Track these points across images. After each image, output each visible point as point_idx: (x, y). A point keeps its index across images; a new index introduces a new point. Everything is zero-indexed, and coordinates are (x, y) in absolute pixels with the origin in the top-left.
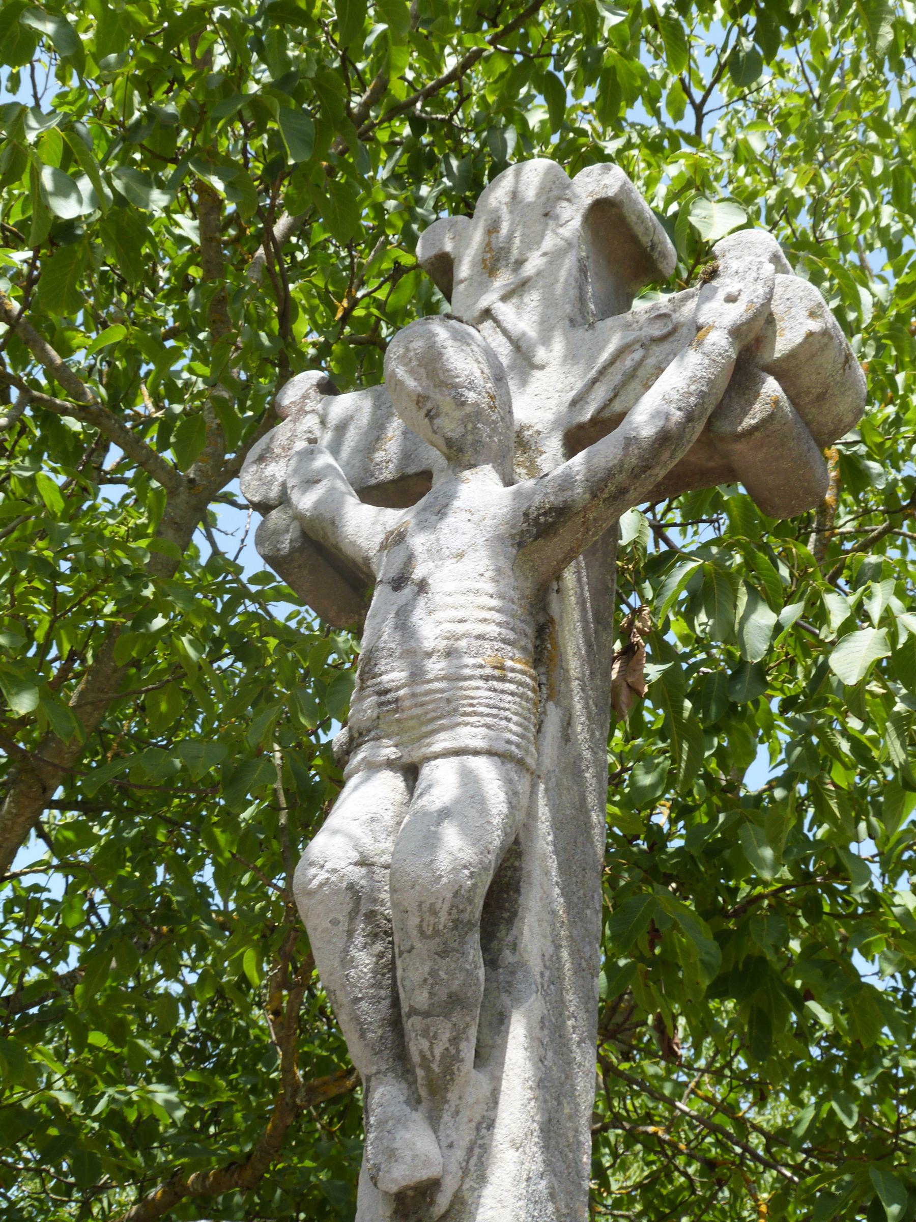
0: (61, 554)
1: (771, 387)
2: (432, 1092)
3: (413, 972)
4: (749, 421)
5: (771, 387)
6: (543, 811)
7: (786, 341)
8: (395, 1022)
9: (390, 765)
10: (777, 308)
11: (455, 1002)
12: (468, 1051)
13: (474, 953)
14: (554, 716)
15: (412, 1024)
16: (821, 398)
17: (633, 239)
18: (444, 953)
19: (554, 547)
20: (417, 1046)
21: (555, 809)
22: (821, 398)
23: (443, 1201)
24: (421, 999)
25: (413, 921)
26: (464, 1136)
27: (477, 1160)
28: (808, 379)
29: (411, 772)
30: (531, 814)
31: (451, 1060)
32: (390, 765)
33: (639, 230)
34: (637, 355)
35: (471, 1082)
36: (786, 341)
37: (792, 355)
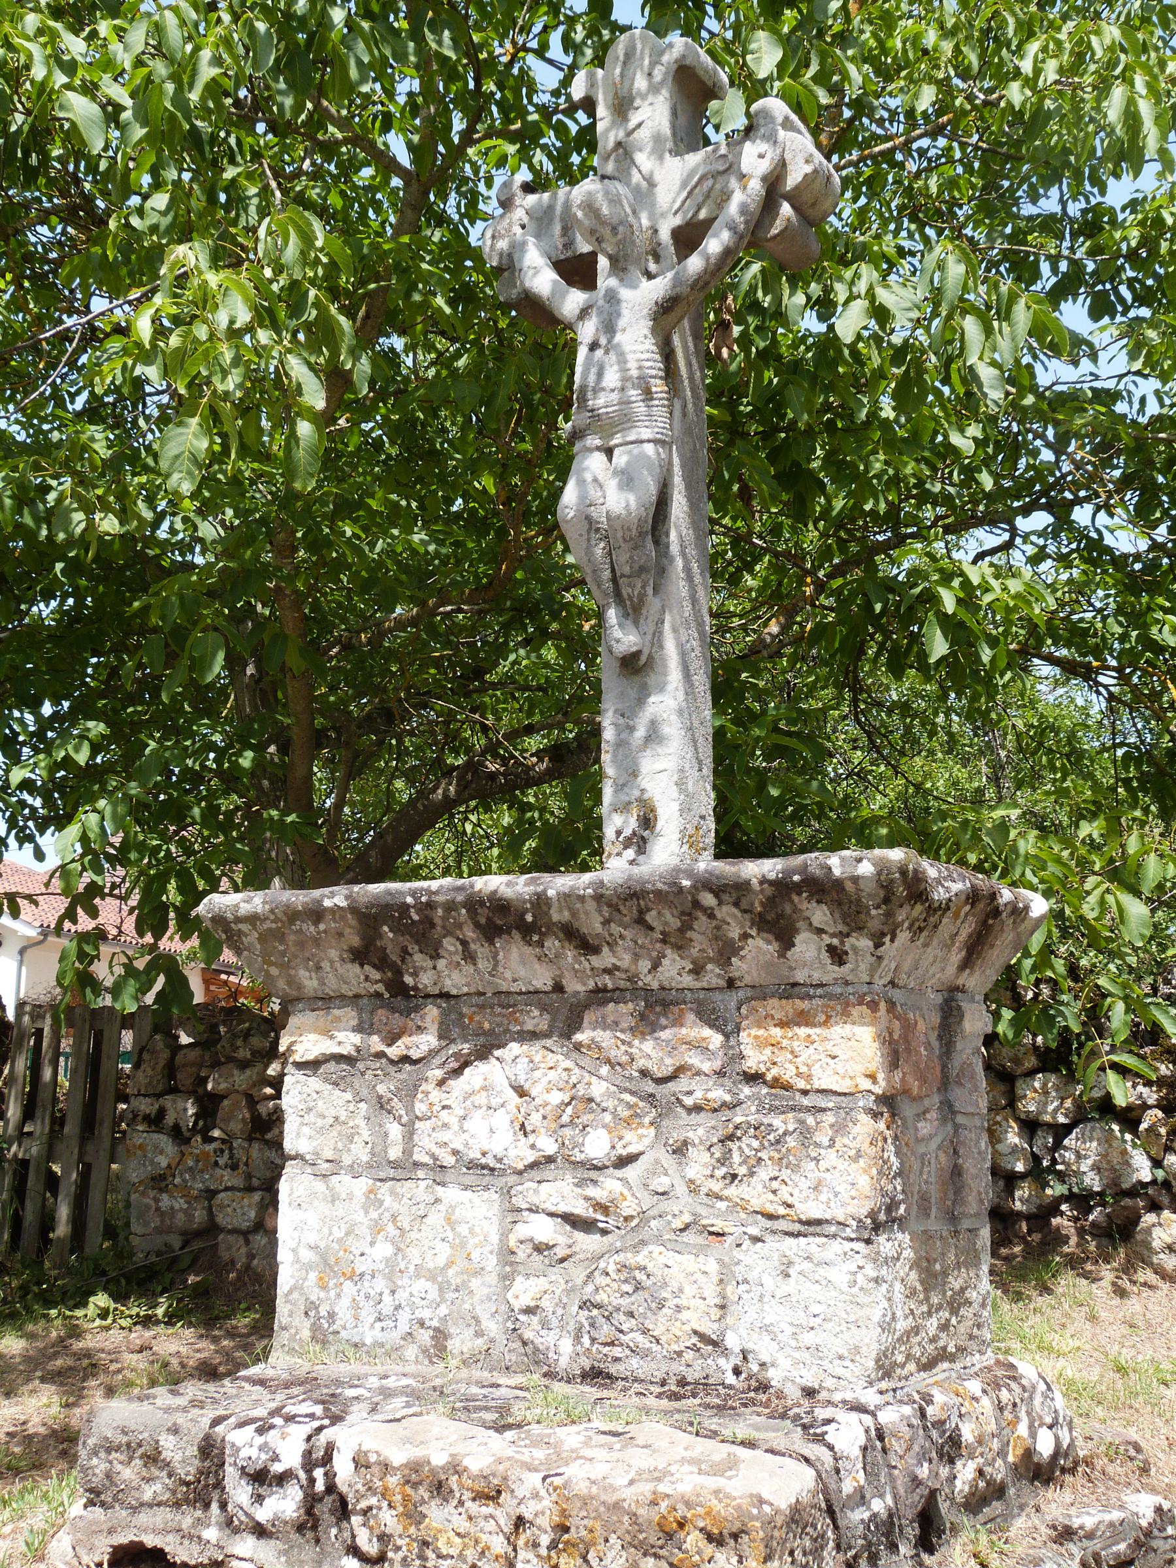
0: (437, 552)
1: (786, 209)
2: (633, 611)
3: (622, 558)
4: (774, 231)
5: (786, 209)
6: (676, 460)
7: (793, 179)
8: (614, 579)
9: (598, 449)
10: (788, 156)
11: (643, 569)
12: (650, 591)
13: (650, 545)
14: (677, 404)
15: (622, 581)
16: (814, 205)
17: (702, 83)
18: (635, 548)
19: (672, 317)
20: (626, 591)
21: (681, 456)
22: (814, 205)
23: (643, 658)
24: (627, 570)
25: (620, 534)
26: (651, 629)
27: (657, 639)
28: (807, 197)
29: (609, 452)
30: (670, 463)
31: (642, 596)
32: (598, 449)
33: (705, 79)
34: (710, 183)
35: (653, 604)
36: (793, 179)
37: (797, 188)
